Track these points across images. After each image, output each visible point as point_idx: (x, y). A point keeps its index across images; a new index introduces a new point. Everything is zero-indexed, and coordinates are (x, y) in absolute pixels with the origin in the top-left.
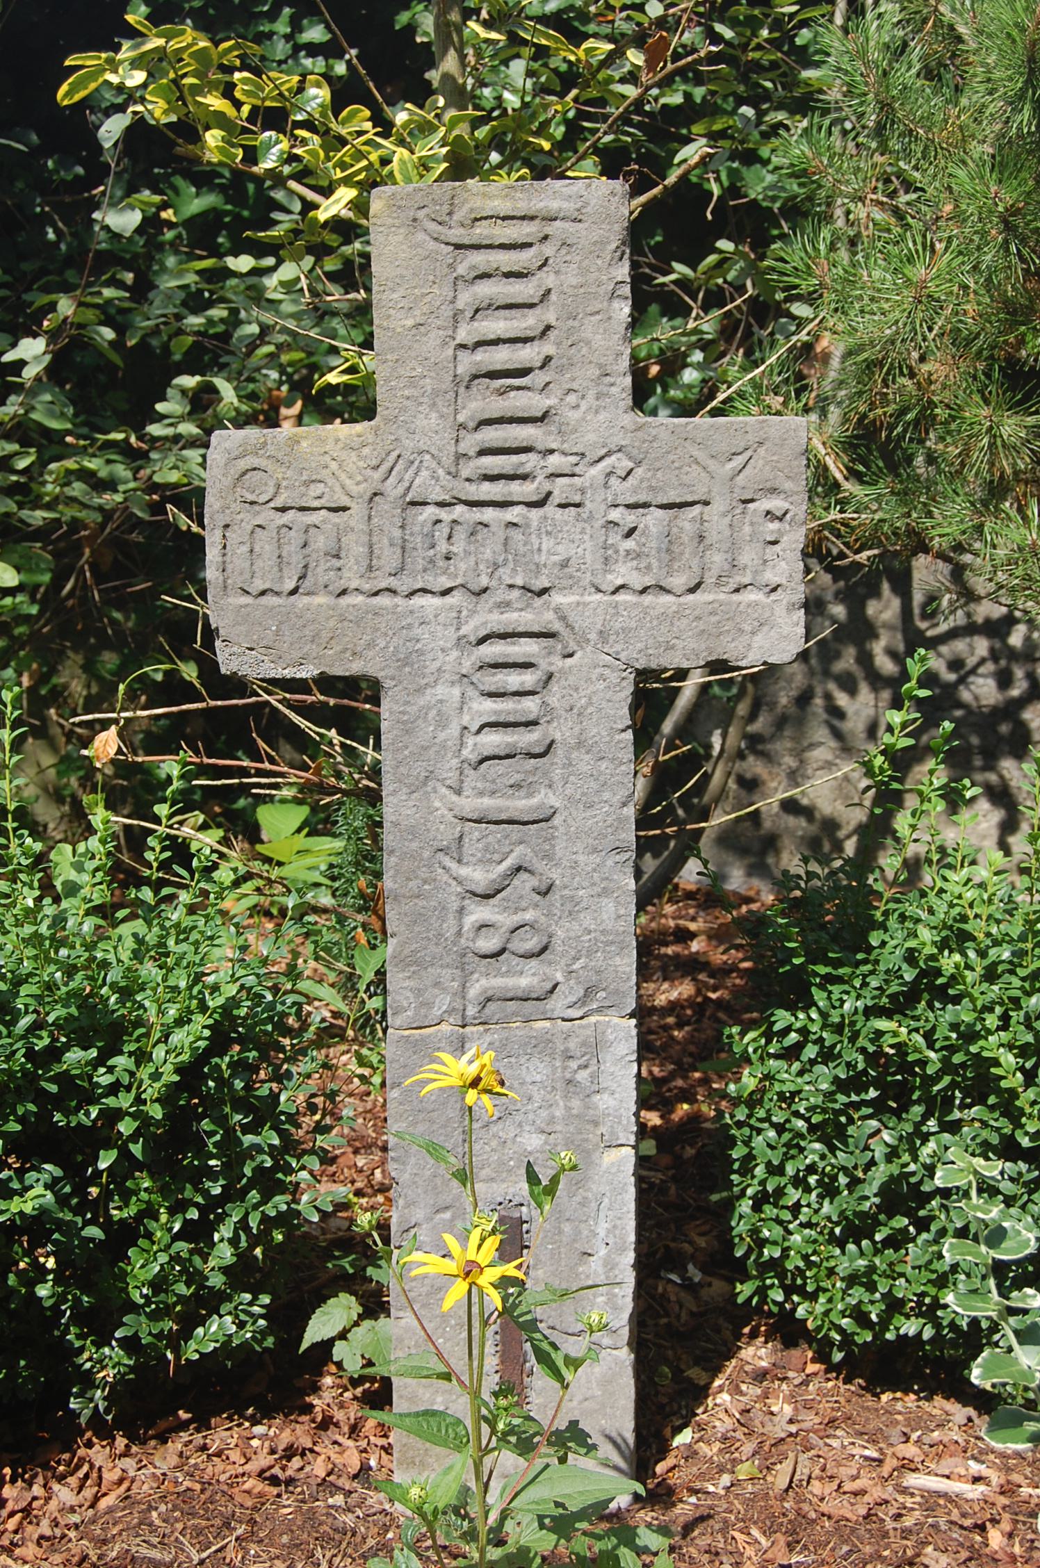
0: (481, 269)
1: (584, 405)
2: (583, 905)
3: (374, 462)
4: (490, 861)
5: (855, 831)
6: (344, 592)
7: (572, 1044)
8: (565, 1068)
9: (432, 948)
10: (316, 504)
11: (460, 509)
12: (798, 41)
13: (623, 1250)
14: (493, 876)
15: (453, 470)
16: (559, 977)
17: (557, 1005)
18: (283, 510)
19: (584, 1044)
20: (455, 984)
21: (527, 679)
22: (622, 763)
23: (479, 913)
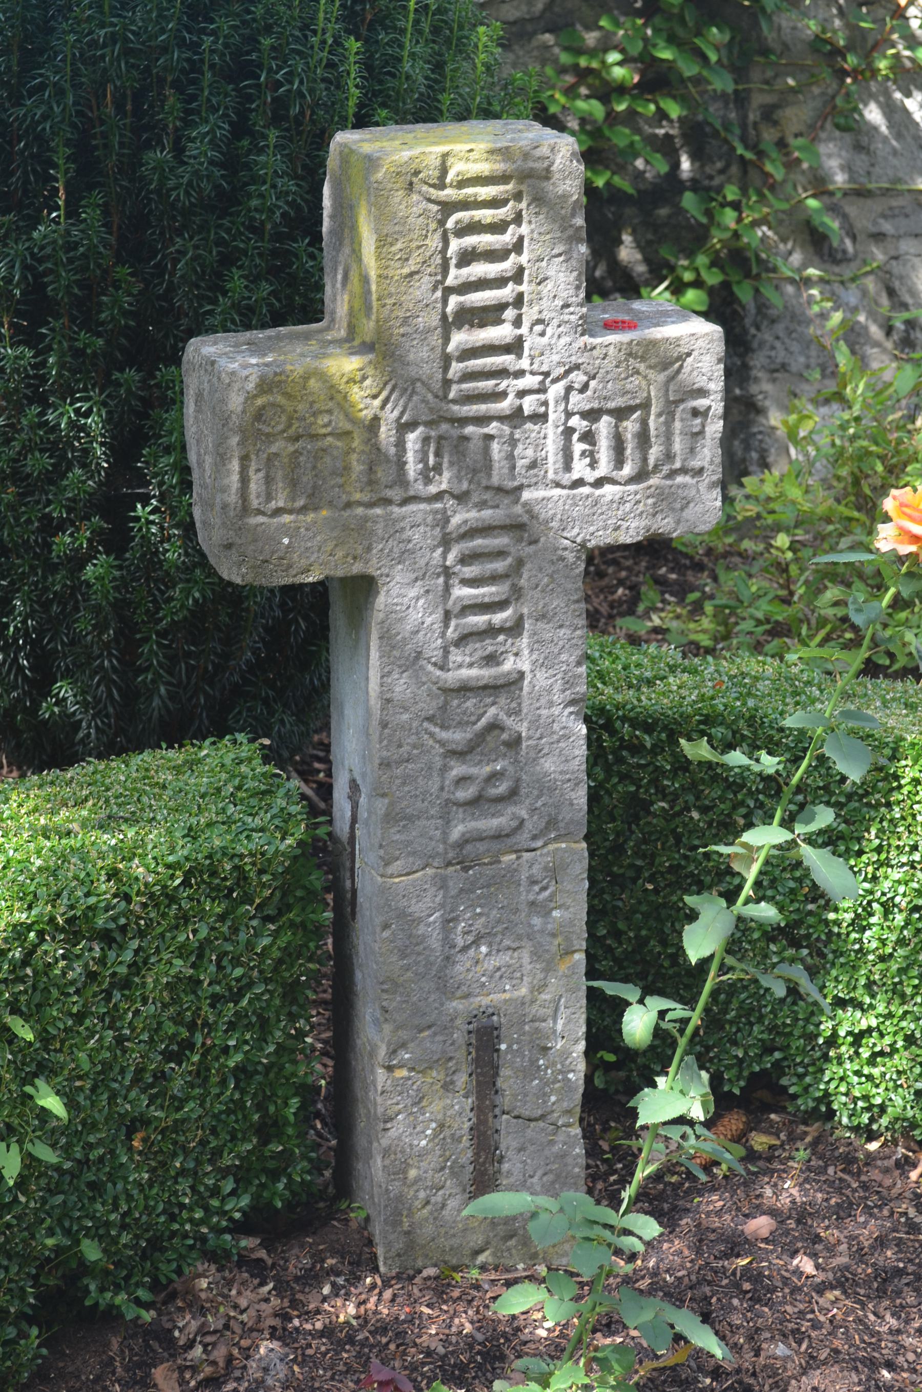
0: (451, 205)
1: (549, 331)
2: (545, 751)
3: (374, 391)
4: (467, 723)
5: (504, 321)
6: (348, 505)
7: (535, 870)
8: (528, 892)
9: (419, 804)
10: (323, 431)
11: (444, 427)
12: (231, 1179)
13: (576, 1041)
14: (469, 736)
15: (440, 394)
16: (524, 814)
17: (523, 838)
18: (297, 438)
19: (546, 869)
20: (438, 833)
21: (500, 566)
22: (576, 629)
23: (458, 770)
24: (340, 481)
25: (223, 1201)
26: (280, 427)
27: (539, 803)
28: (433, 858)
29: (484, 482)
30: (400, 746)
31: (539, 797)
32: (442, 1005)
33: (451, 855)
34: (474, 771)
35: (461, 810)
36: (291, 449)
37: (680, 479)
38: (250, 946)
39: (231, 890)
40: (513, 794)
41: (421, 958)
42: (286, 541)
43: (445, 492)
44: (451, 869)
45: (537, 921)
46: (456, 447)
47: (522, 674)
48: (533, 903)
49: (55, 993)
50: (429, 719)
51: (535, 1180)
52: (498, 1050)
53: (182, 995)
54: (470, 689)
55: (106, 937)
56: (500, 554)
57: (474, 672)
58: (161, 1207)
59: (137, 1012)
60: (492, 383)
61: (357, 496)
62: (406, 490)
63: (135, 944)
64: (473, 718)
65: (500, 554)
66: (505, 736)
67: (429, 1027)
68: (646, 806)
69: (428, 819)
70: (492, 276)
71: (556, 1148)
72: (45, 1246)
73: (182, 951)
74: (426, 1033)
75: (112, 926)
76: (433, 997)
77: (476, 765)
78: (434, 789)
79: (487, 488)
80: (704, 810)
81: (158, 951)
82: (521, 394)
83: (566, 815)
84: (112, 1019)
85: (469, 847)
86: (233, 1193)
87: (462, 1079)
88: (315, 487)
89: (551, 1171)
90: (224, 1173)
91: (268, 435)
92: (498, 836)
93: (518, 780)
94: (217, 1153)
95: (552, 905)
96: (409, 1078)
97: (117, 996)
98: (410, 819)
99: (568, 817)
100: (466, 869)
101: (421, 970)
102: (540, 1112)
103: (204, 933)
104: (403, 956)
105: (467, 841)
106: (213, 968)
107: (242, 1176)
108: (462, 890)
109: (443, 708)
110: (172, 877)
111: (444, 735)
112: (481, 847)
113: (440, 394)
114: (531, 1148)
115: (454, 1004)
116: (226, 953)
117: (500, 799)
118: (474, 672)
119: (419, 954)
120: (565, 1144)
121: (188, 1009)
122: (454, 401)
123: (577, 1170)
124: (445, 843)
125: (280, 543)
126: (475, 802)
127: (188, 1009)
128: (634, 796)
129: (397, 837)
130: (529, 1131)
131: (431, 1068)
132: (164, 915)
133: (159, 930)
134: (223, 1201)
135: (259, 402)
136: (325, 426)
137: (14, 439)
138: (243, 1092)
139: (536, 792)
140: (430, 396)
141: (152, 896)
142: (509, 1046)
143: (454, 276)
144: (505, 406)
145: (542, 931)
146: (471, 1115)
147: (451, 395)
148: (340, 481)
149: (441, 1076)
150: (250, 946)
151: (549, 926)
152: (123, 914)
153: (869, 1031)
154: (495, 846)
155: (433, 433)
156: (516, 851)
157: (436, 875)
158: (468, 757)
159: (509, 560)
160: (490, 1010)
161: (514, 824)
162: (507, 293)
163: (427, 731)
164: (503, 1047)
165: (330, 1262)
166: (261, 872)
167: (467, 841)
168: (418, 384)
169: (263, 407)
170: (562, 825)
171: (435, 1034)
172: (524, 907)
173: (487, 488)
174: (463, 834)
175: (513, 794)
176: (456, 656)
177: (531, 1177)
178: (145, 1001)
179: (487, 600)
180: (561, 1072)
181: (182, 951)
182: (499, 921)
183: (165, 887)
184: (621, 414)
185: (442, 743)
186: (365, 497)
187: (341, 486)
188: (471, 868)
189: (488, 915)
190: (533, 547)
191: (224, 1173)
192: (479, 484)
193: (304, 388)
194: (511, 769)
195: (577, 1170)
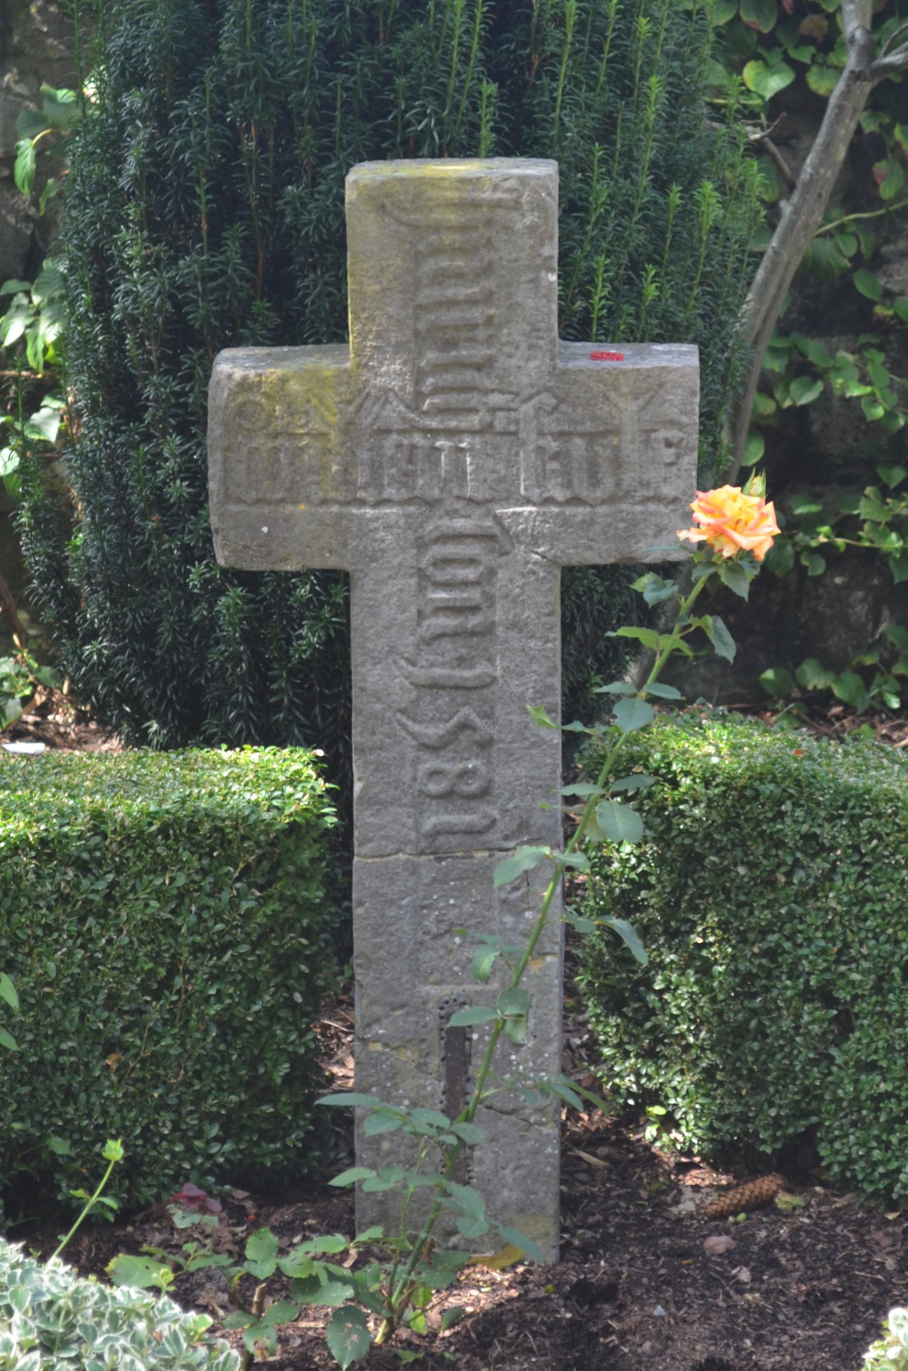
4: (440, 720)
9: (392, 791)
10: (301, 431)
14: (441, 732)
15: (413, 405)
16: (496, 814)
17: (494, 837)
18: (276, 435)
21: (470, 573)
23: (431, 763)
24: (317, 478)
25: (208, 1143)
26: (260, 424)
27: (511, 805)
28: (406, 844)
29: (456, 492)
30: (373, 734)
31: (511, 799)
32: (414, 986)
33: (423, 844)
34: (447, 766)
35: (434, 802)
36: (270, 445)
37: (652, 507)
38: (233, 904)
39: (213, 850)
40: (485, 793)
41: (393, 938)
42: (265, 529)
43: (416, 497)
44: (424, 858)
45: (509, 919)
46: (428, 456)
47: (494, 679)
48: (504, 902)
49: (24, 901)
50: (403, 711)
51: (507, 1172)
52: (470, 1039)
53: (161, 937)
54: (443, 687)
55: (83, 868)
56: (472, 561)
57: (445, 672)
58: (138, 1131)
59: (110, 942)
60: (463, 397)
61: (332, 494)
62: (380, 492)
63: (110, 877)
64: (445, 716)
65: (472, 561)
66: (477, 737)
67: (402, 1006)
68: (700, 858)
69: (400, 806)
70: (462, 297)
71: (529, 1144)
72: (11, 1129)
73: (159, 893)
74: (399, 1012)
75: (85, 856)
76: (405, 978)
77: (448, 761)
78: (407, 778)
79: (459, 498)
80: (752, 866)
81: (133, 889)
82: (494, 410)
83: (538, 820)
84: (87, 940)
85: (441, 840)
86: (216, 1139)
87: (435, 1062)
88: (293, 482)
89: (523, 1166)
90: (213, 1118)
91: (248, 430)
92: (469, 832)
93: (490, 781)
94: (200, 1097)
95: (524, 906)
96: (382, 1053)
97: (91, 921)
98: (384, 804)
99: (540, 822)
100: (439, 860)
101: (394, 950)
102: (511, 1106)
103: (181, 880)
104: (376, 934)
105: (439, 833)
106: (193, 919)
107: (231, 1128)
108: (435, 880)
109: (415, 702)
110: (150, 824)
111: (417, 728)
112: (454, 840)
113: (413, 405)
114: (503, 1140)
115: (427, 988)
116: (207, 908)
117: (472, 797)
118: (445, 672)
119: (392, 934)
120: (537, 1141)
121: (167, 951)
122: (426, 413)
123: (549, 1169)
124: (417, 831)
125: (260, 531)
126: (447, 796)
127: (167, 951)
128: (691, 848)
129: (371, 820)
130: (501, 1123)
131: (405, 1047)
132: (140, 857)
133: (135, 869)
134: (208, 1143)
135: (240, 399)
136: (302, 426)
137: (160, 468)
138: (229, 1045)
139: (507, 794)
140: (402, 408)
141: (128, 837)
142: (481, 1037)
143: (428, 294)
144: (474, 421)
145: (514, 930)
146: (443, 1098)
147: (425, 407)
148: (317, 478)
149: (416, 1057)
150: (233, 904)
151: (521, 926)
152: (97, 848)
153: (888, 1095)
154: (468, 840)
155: (406, 442)
156: (489, 849)
157: (408, 861)
158: (442, 753)
159: (481, 568)
160: (462, 999)
161: (485, 822)
162: (477, 314)
163: (399, 722)
164: (475, 1036)
165: (311, 1221)
166: (244, 838)
167: (439, 833)
168: (391, 394)
169: (244, 404)
170: (534, 829)
171: (408, 1014)
172: (496, 904)
173: (459, 498)
174: (435, 826)
175: (485, 793)
176: (426, 657)
177: (503, 1168)
178: (119, 931)
179: (458, 604)
180: (532, 1070)
181: (159, 893)
182: (472, 915)
183: (141, 833)
184: (591, 437)
185: (414, 736)
186: (340, 495)
187: (318, 483)
188: (443, 859)
189: (460, 907)
190: (504, 558)
191: (213, 1118)
192: (450, 493)
193: (282, 389)
194: (483, 769)
195: (549, 1169)
